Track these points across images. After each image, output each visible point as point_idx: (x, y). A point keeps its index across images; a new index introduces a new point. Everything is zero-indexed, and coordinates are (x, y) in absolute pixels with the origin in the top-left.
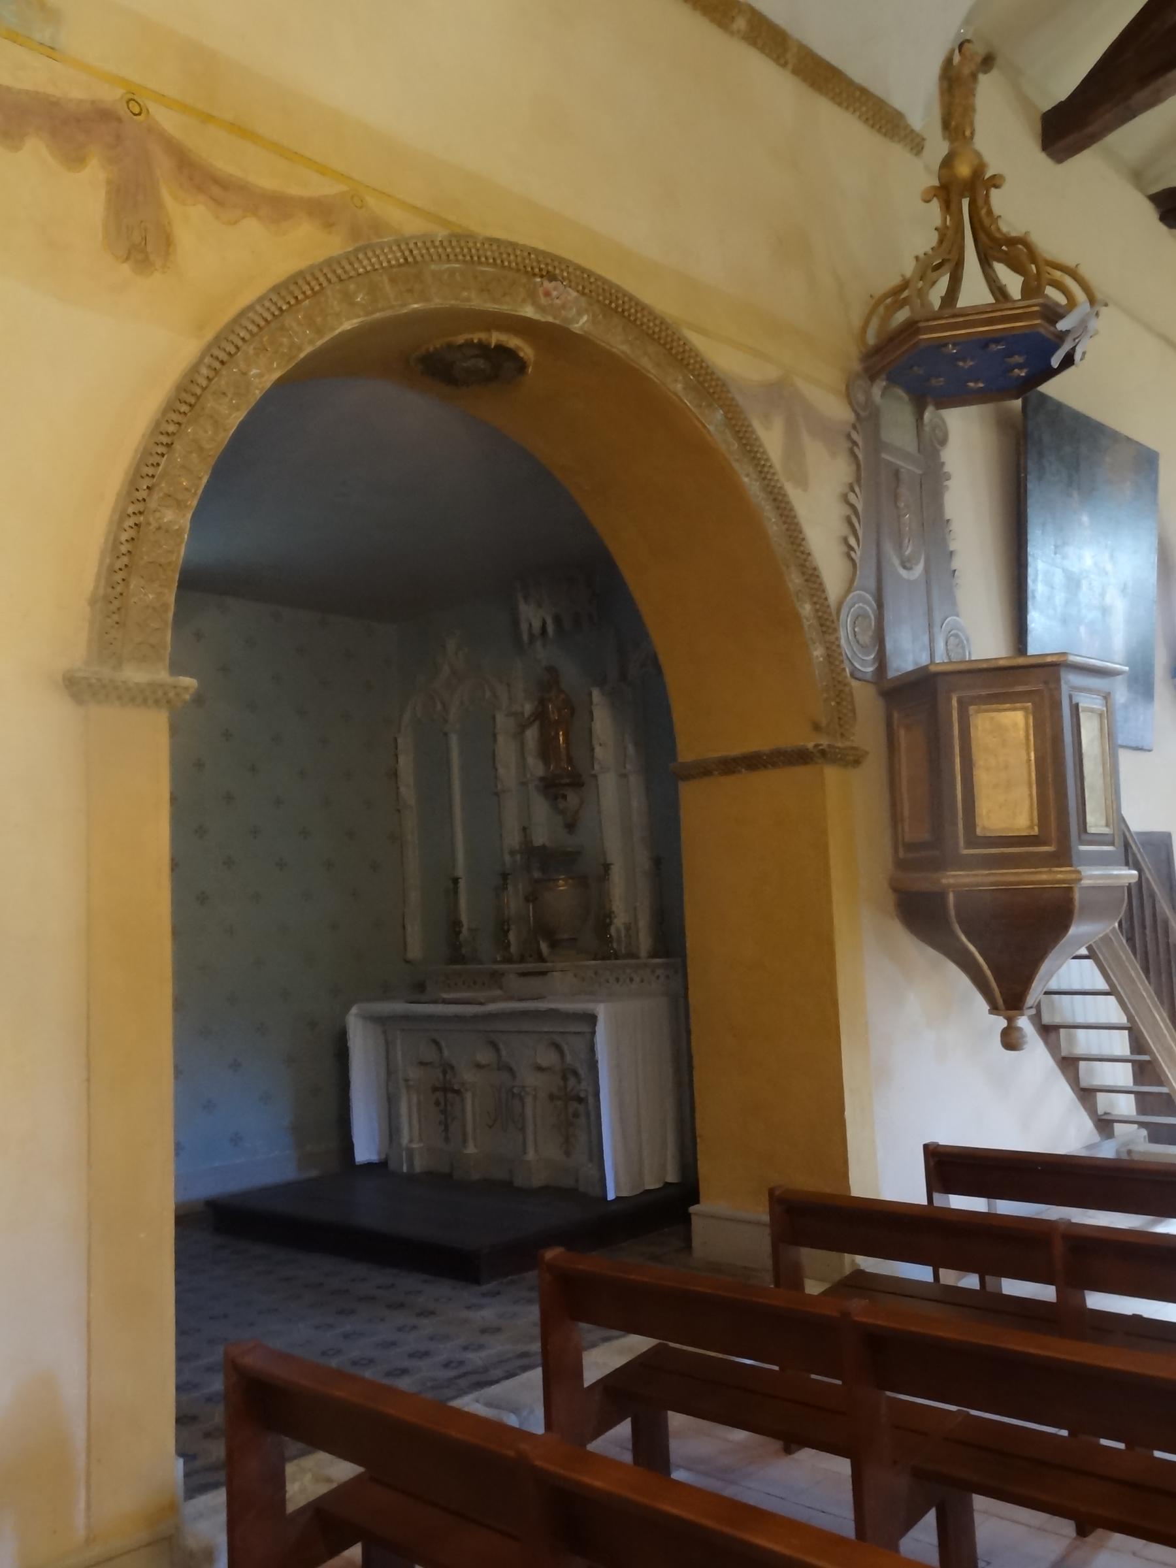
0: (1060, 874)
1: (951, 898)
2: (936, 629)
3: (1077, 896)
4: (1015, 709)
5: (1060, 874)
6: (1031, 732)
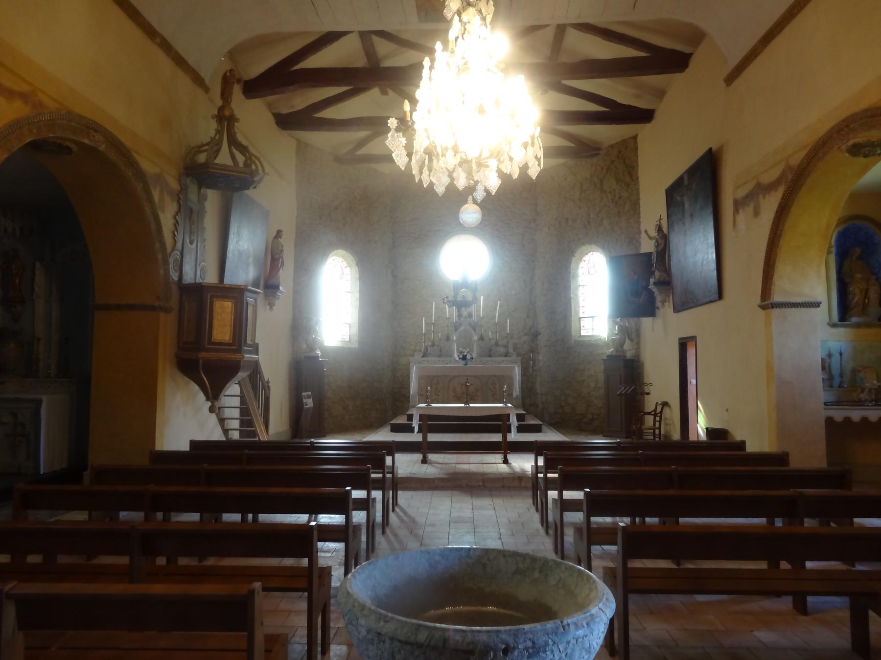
0: (238, 356)
1: (201, 362)
2: (198, 266)
3: (242, 363)
4: (228, 301)
5: (238, 356)
6: (233, 309)
